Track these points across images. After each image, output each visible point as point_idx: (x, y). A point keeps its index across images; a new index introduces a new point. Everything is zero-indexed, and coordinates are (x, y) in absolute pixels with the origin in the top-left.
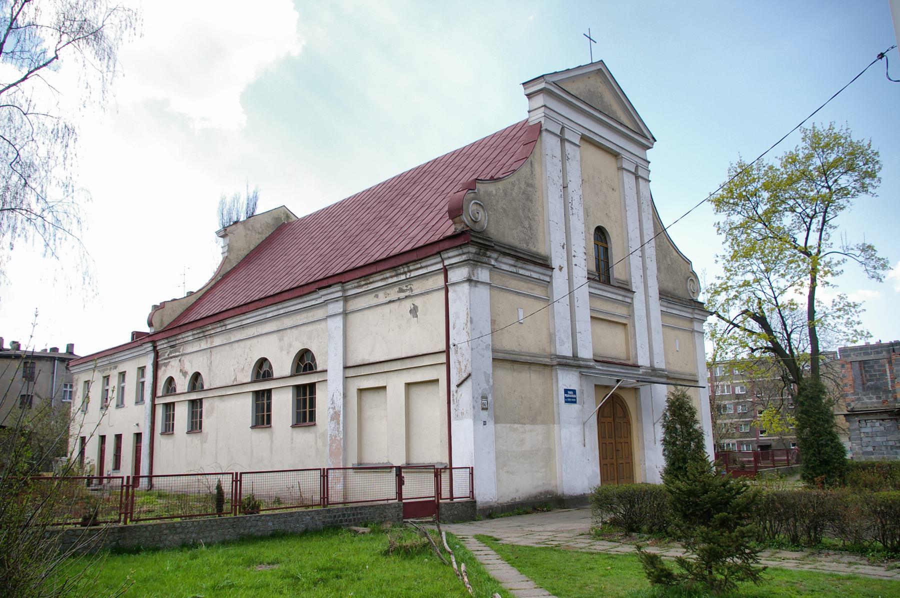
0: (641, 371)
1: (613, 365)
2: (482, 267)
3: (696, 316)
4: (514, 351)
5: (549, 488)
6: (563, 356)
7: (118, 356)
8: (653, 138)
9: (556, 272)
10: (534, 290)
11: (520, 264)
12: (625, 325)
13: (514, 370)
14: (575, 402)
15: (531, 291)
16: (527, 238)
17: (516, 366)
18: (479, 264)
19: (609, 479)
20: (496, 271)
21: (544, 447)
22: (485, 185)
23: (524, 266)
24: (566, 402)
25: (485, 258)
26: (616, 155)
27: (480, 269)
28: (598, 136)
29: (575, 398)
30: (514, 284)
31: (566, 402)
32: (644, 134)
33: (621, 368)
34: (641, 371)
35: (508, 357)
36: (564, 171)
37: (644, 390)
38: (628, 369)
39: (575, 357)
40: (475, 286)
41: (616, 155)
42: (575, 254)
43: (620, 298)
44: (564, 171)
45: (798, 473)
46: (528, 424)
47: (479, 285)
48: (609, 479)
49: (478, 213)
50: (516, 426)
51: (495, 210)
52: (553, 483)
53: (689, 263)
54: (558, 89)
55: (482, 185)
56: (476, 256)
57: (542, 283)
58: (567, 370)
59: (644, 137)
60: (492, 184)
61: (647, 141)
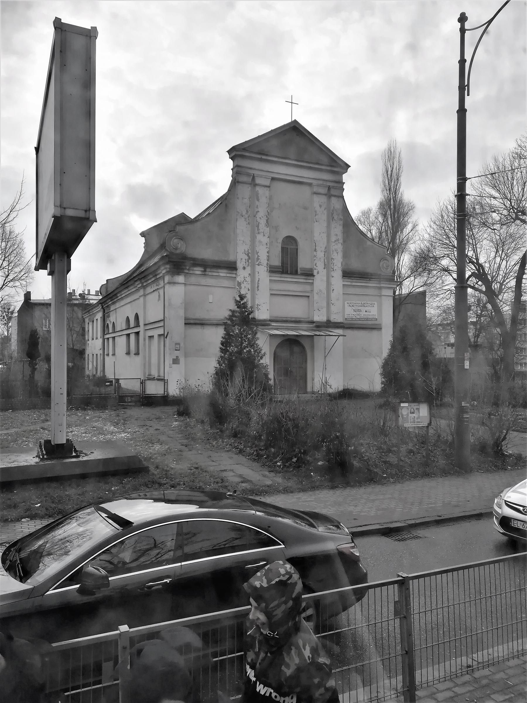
3: (382, 285)
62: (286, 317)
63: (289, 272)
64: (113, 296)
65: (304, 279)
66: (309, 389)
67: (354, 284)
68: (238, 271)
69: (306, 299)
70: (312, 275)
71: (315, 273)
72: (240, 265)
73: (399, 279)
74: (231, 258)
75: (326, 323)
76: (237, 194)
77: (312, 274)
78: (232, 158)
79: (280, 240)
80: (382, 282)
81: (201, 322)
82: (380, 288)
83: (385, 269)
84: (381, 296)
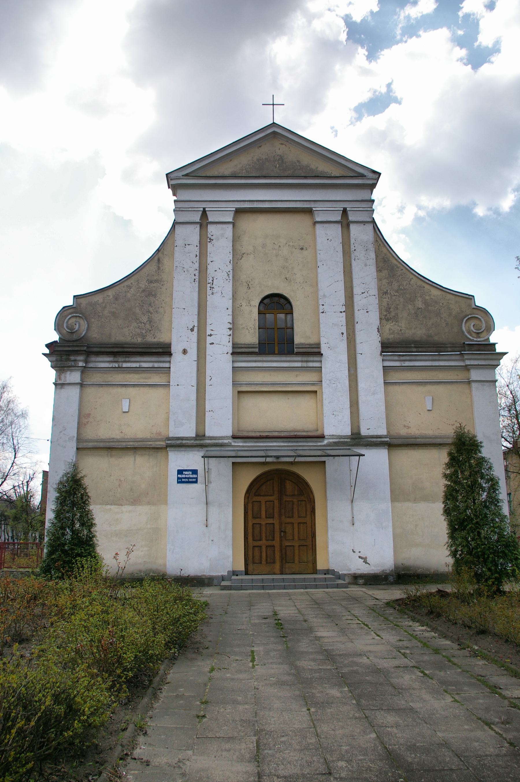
0: (326, 442)
1: (268, 440)
2: (71, 371)
3: (468, 362)
4: (113, 439)
5: (154, 567)
6: (177, 437)
7: (212, 449)
8: (374, 172)
9: (177, 356)
10: (150, 378)
11: (120, 359)
12: (316, 392)
13: (111, 456)
14: (196, 482)
15: (144, 380)
16: (144, 332)
17: (114, 453)
18: (66, 368)
19: (264, 562)
20: (93, 371)
21: (149, 526)
22: (88, 298)
23: (127, 359)
24: (178, 482)
25: (71, 362)
26: (309, 211)
27: (68, 373)
28: (267, 203)
29: (197, 478)
30: (119, 378)
31: (178, 482)
32: (359, 173)
33: (283, 442)
34: (326, 442)
35: (102, 445)
36: (203, 254)
37: (331, 465)
38: (297, 442)
39: (200, 436)
40: (61, 388)
41: (309, 211)
42: (212, 333)
43: (299, 364)
44: (203, 254)
45: (105, 579)
46: (126, 505)
47: (66, 387)
48: (264, 562)
49: (76, 324)
50: (109, 507)
51: (99, 316)
52: (160, 561)
53: (470, 298)
54: (193, 179)
55: (83, 299)
56: (60, 363)
57: (158, 370)
58: (185, 451)
59: (362, 176)
60: (100, 294)
61: (363, 179)
62: (307, 431)
63: (276, 352)
64: (495, 731)
65: (302, 361)
66: (320, 566)
67: (407, 364)
68: (173, 359)
69: (313, 395)
70: (320, 354)
71: (324, 350)
72: (176, 349)
73: (18, 433)
74: (163, 338)
75: (352, 439)
76: (260, 147)
77: (320, 352)
78: (175, 188)
79: (256, 302)
80: (466, 357)
81: (107, 445)
82: (467, 368)
83: (474, 335)
84: (469, 382)
